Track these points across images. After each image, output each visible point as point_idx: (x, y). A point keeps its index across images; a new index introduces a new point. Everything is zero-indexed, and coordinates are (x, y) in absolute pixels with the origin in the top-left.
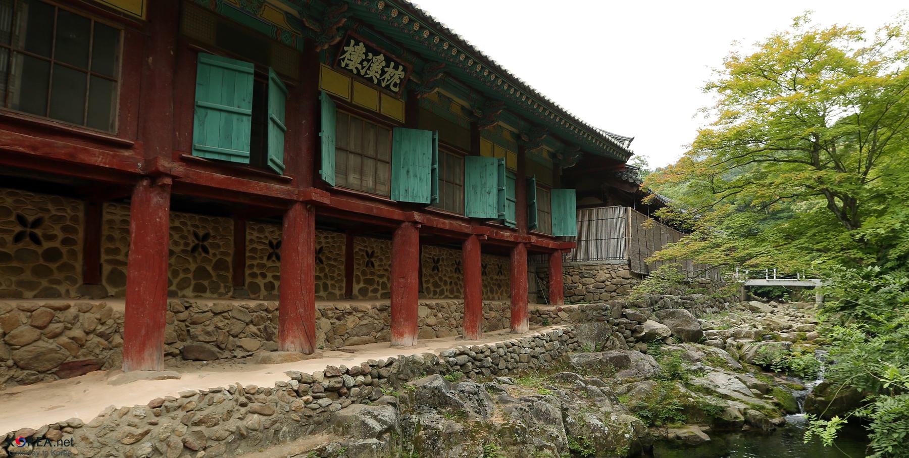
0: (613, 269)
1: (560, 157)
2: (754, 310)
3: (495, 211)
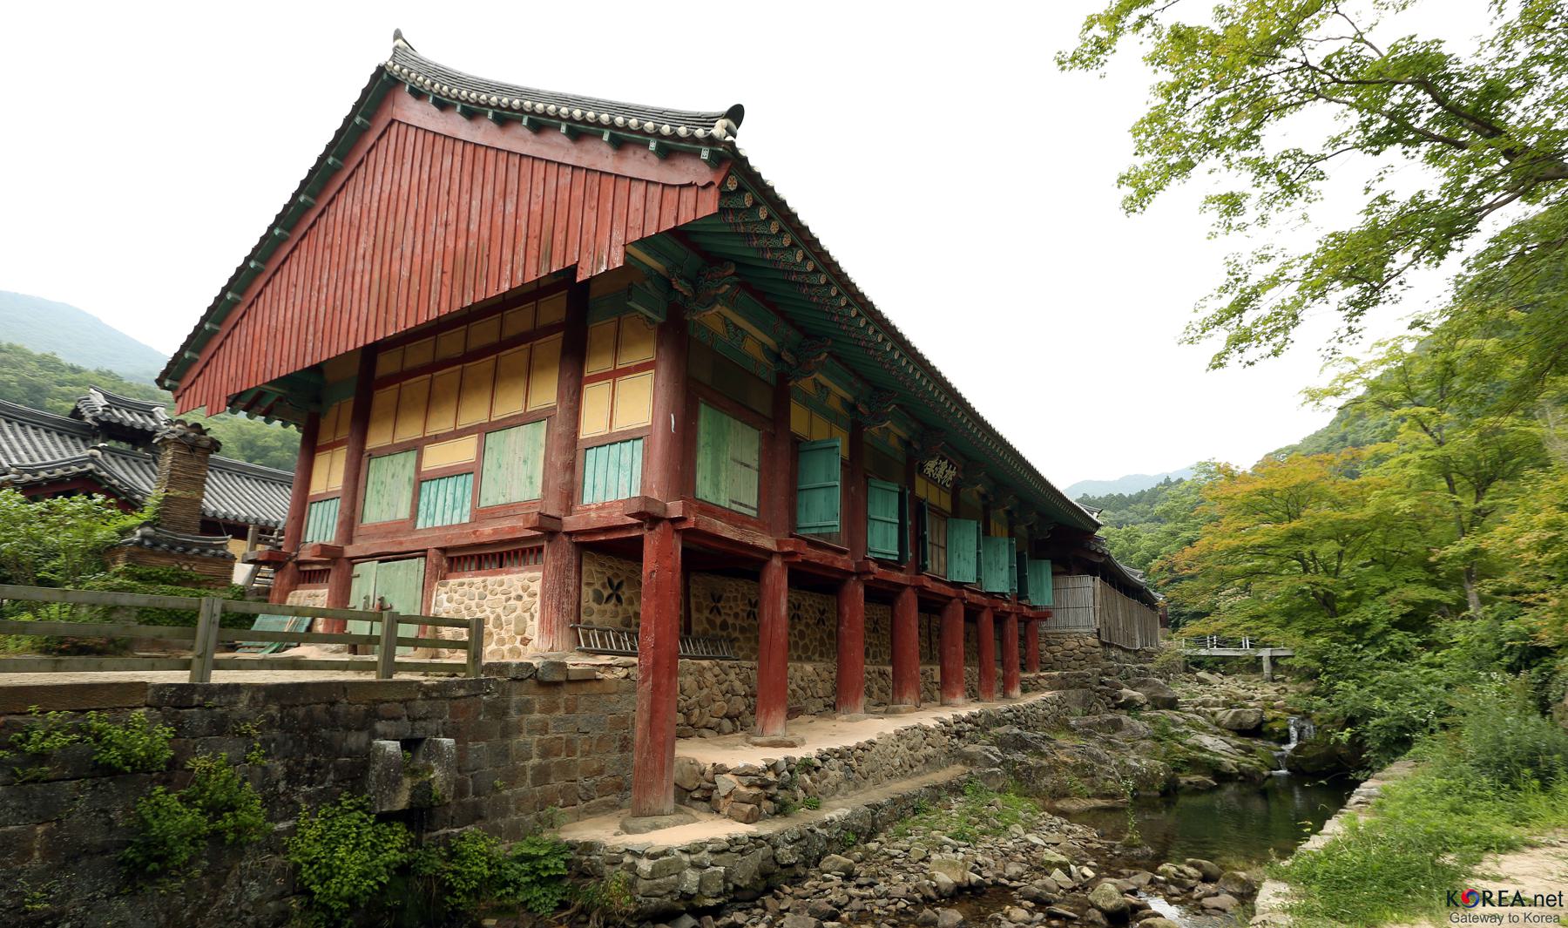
1: (916, 446)
2: (1201, 681)
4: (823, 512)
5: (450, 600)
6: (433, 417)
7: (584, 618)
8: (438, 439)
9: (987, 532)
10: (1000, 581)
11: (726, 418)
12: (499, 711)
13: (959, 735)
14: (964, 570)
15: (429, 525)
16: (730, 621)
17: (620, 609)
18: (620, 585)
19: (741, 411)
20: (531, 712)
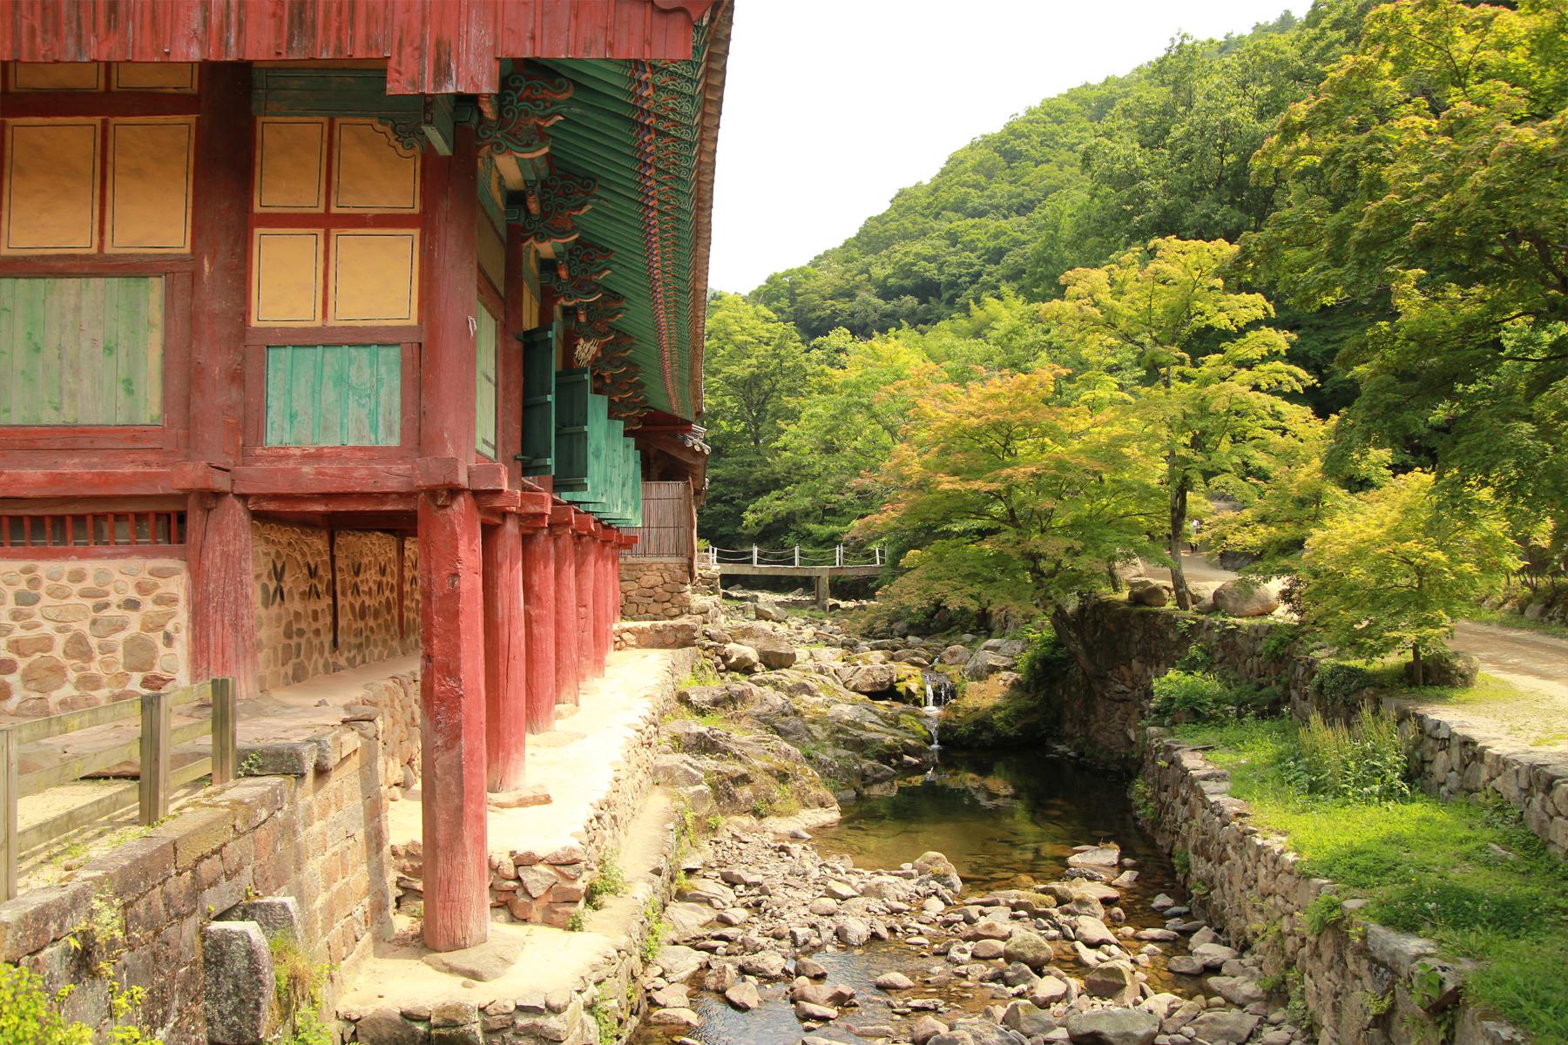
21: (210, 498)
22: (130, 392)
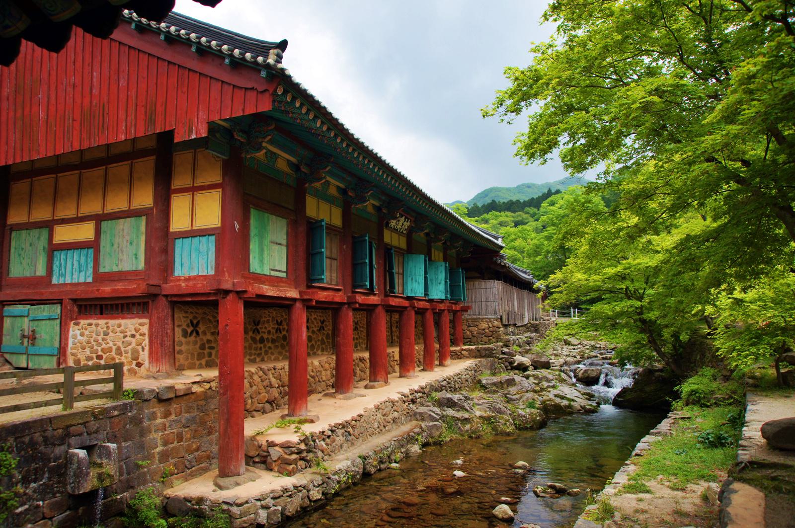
0: (490, 321)
3: (443, 294)
4: (330, 275)
5: (82, 335)
6: (60, 206)
7: (177, 348)
8: (64, 221)
9: (430, 259)
10: (438, 292)
11: (266, 215)
12: (137, 421)
13: (413, 401)
14: (415, 288)
15: (61, 282)
16: (265, 336)
17: (198, 339)
18: (198, 323)
19: (274, 208)
20: (155, 419)
21: (154, 296)
22: (136, 258)
